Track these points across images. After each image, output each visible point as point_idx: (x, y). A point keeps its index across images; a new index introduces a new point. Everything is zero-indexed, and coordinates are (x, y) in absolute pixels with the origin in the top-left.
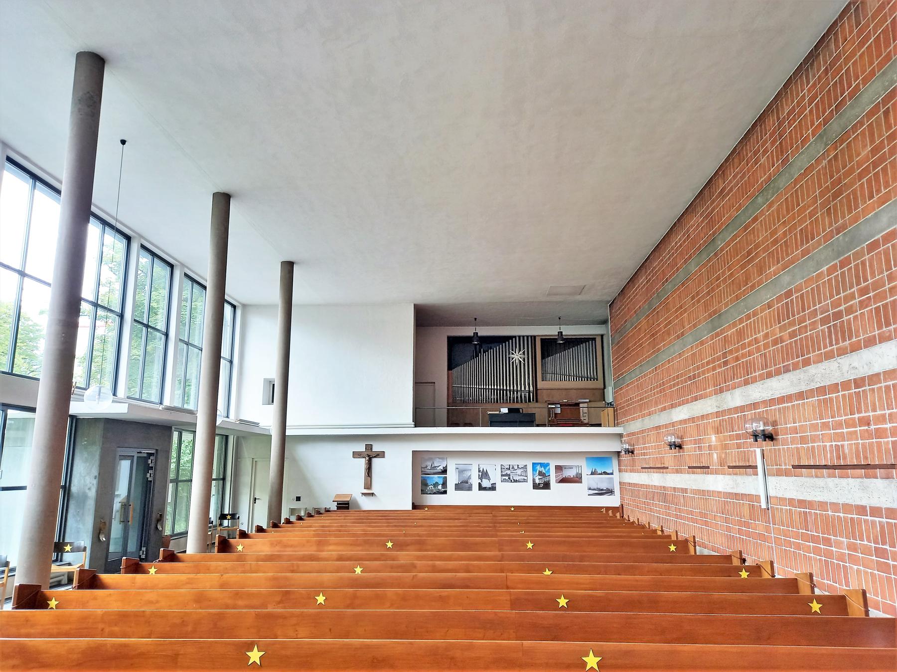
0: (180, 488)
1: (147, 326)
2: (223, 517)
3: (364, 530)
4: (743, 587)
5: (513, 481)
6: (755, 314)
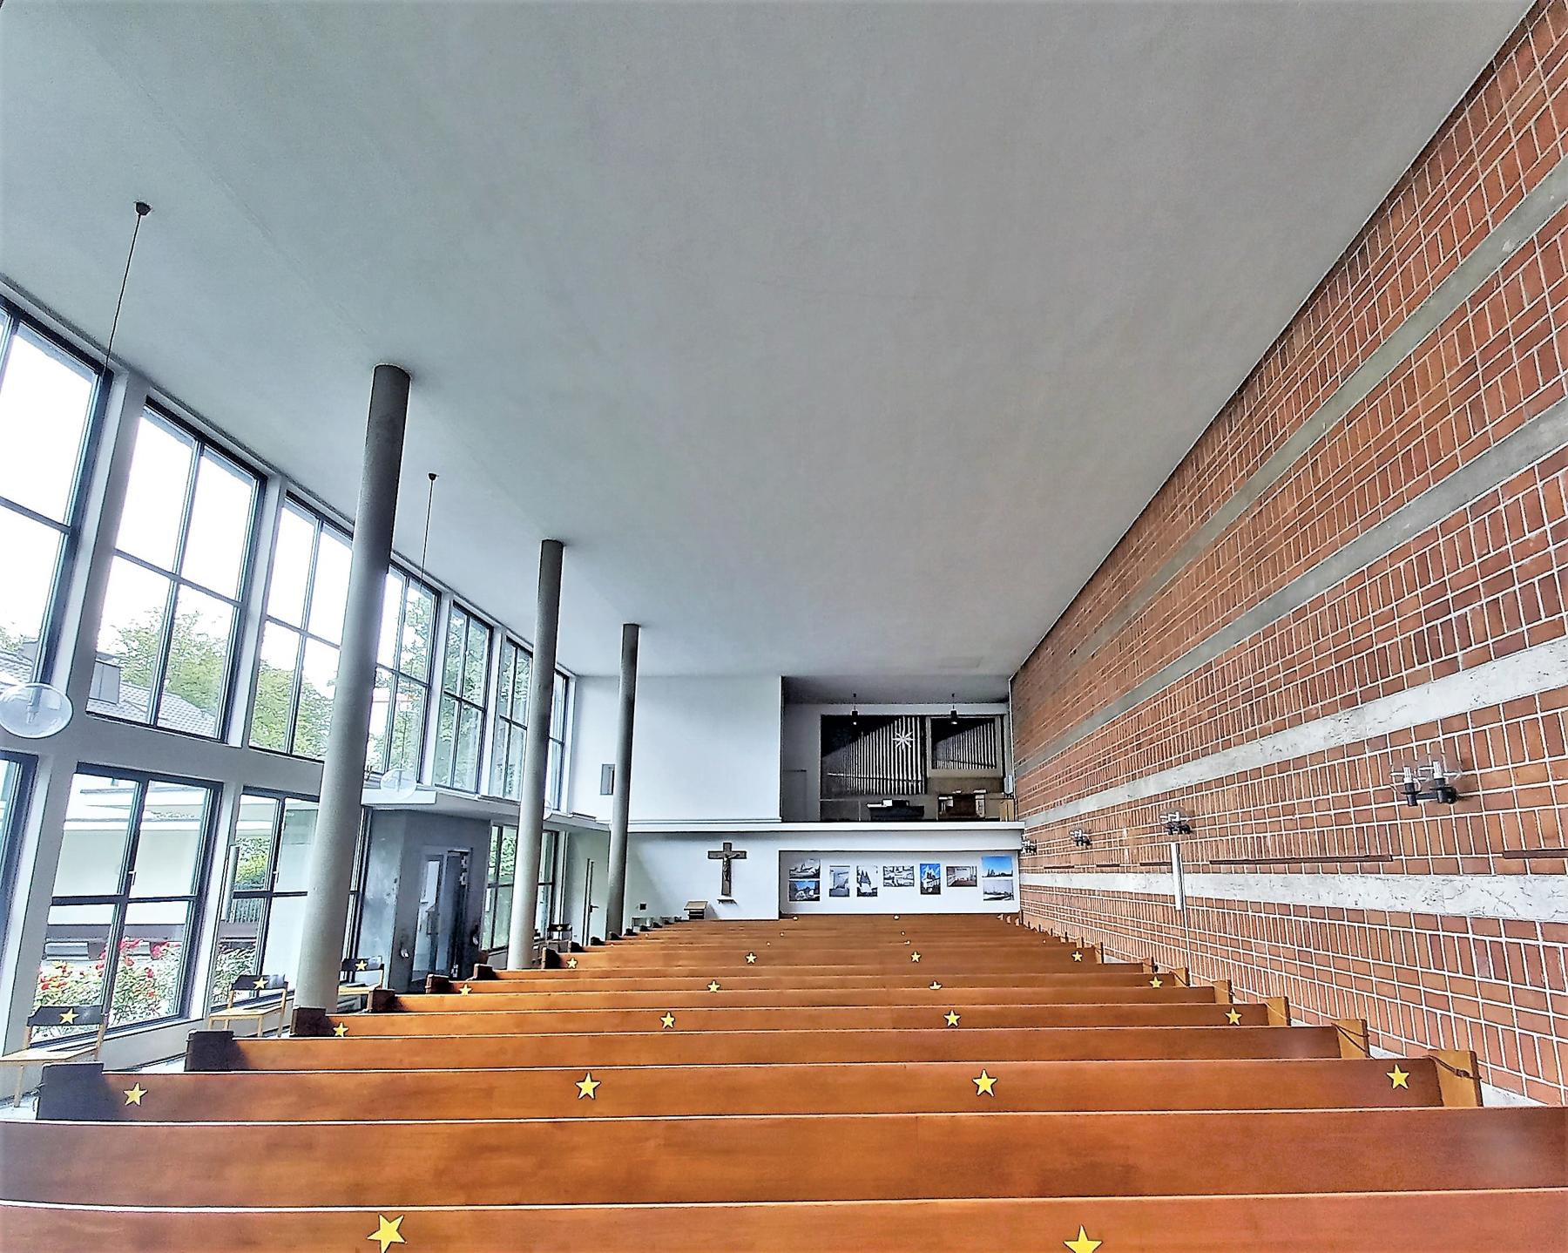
0: (499, 895)
1: (460, 700)
2: (553, 928)
3: (721, 943)
4: (1154, 996)
6: (1171, 690)
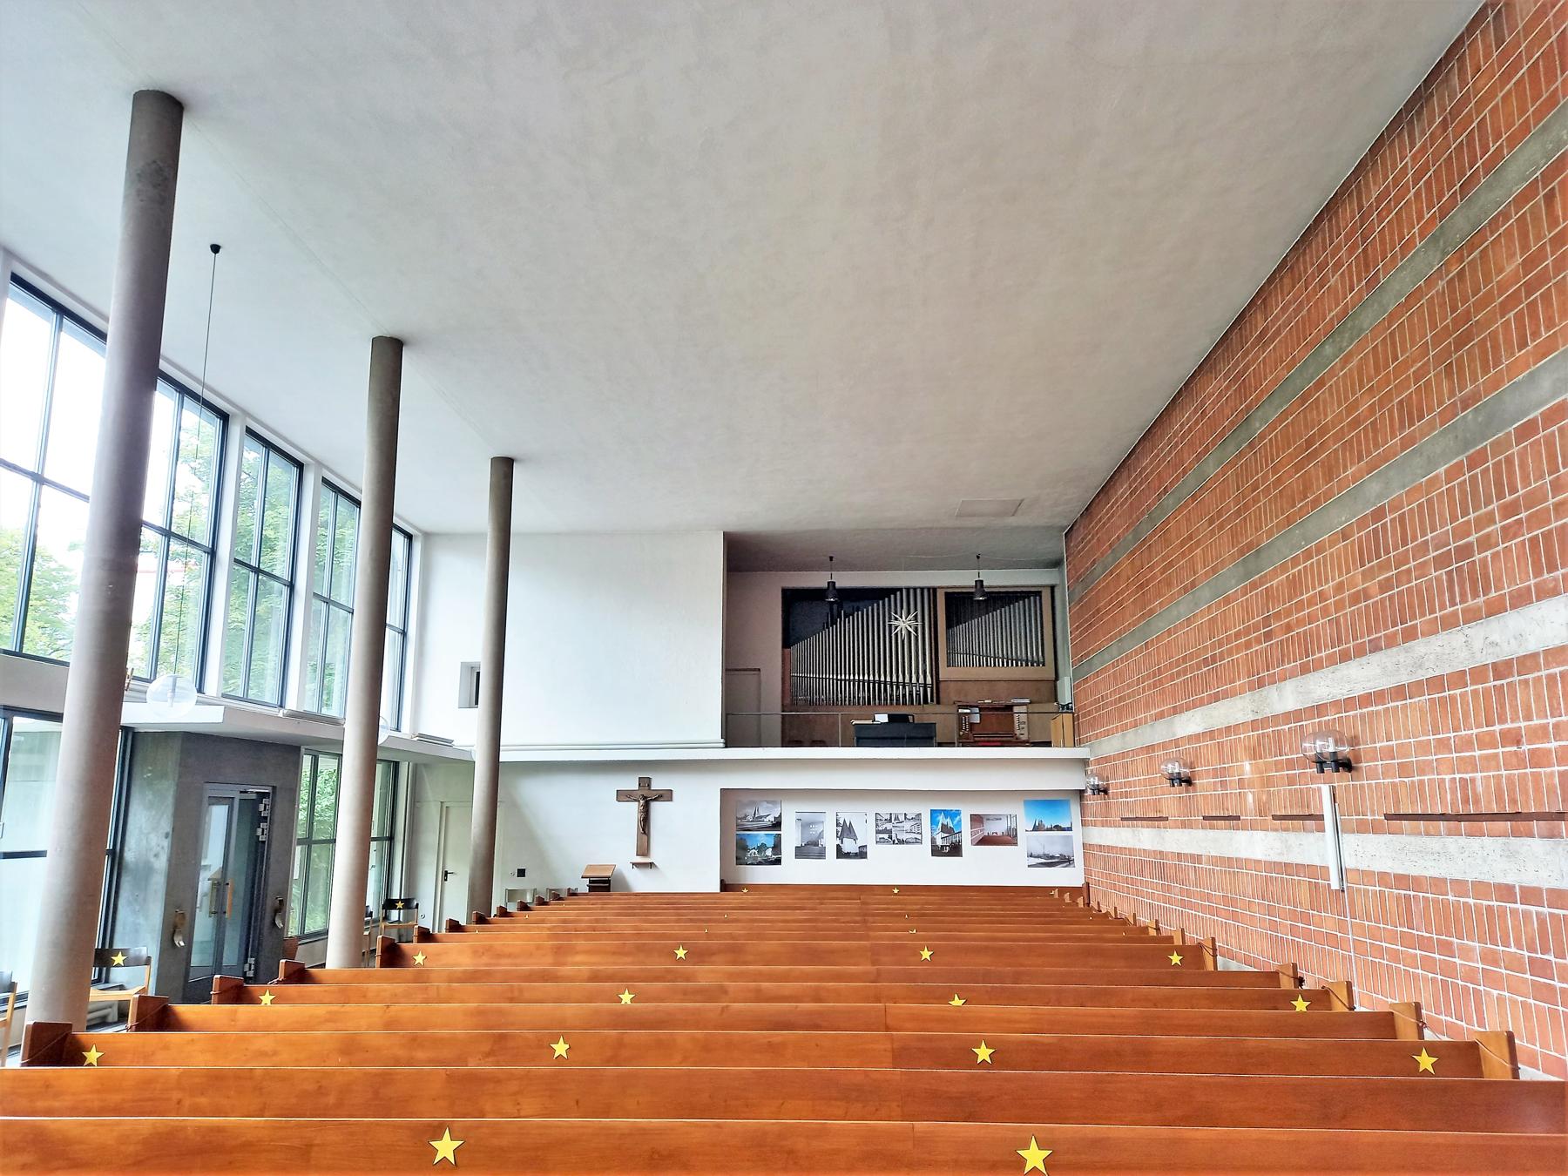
0: (314, 855)
1: (257, 571)
2: (390, 904)
3: (635, 928)
4: (1299, 1027)
5: (896, 841)
6: (1320, 549)
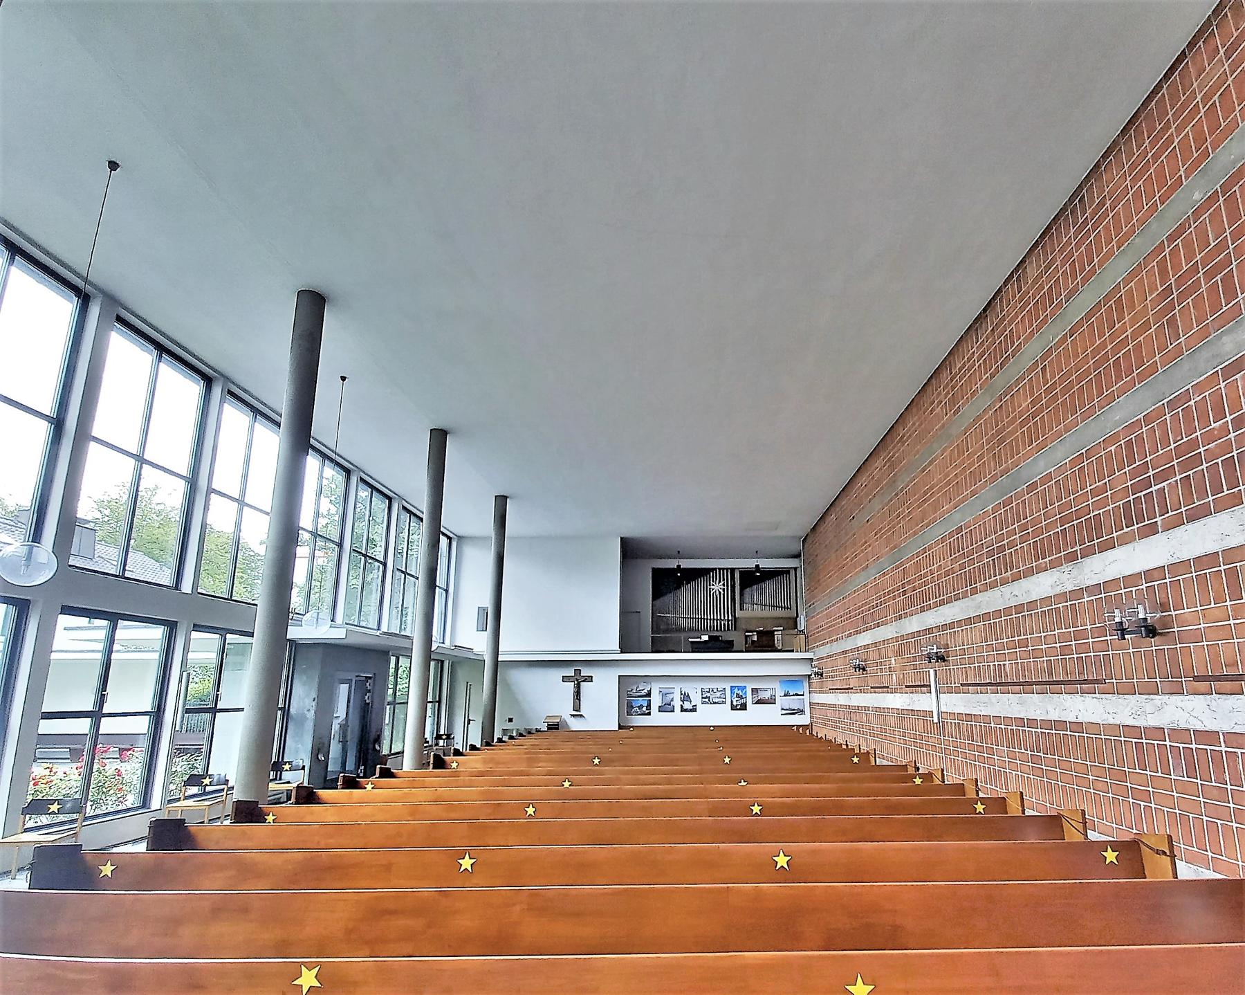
0: (396, 711)
1: (365, 556)
2: (439, 737)
3: (573, 748)
4: (917, 791)
6: (930, 548)
